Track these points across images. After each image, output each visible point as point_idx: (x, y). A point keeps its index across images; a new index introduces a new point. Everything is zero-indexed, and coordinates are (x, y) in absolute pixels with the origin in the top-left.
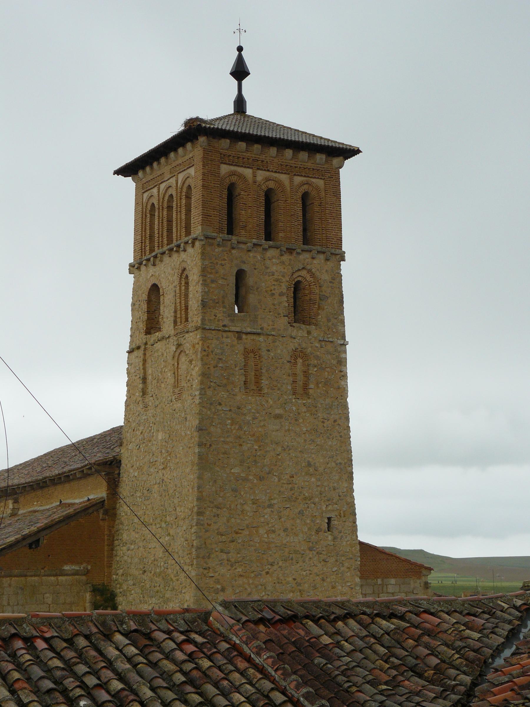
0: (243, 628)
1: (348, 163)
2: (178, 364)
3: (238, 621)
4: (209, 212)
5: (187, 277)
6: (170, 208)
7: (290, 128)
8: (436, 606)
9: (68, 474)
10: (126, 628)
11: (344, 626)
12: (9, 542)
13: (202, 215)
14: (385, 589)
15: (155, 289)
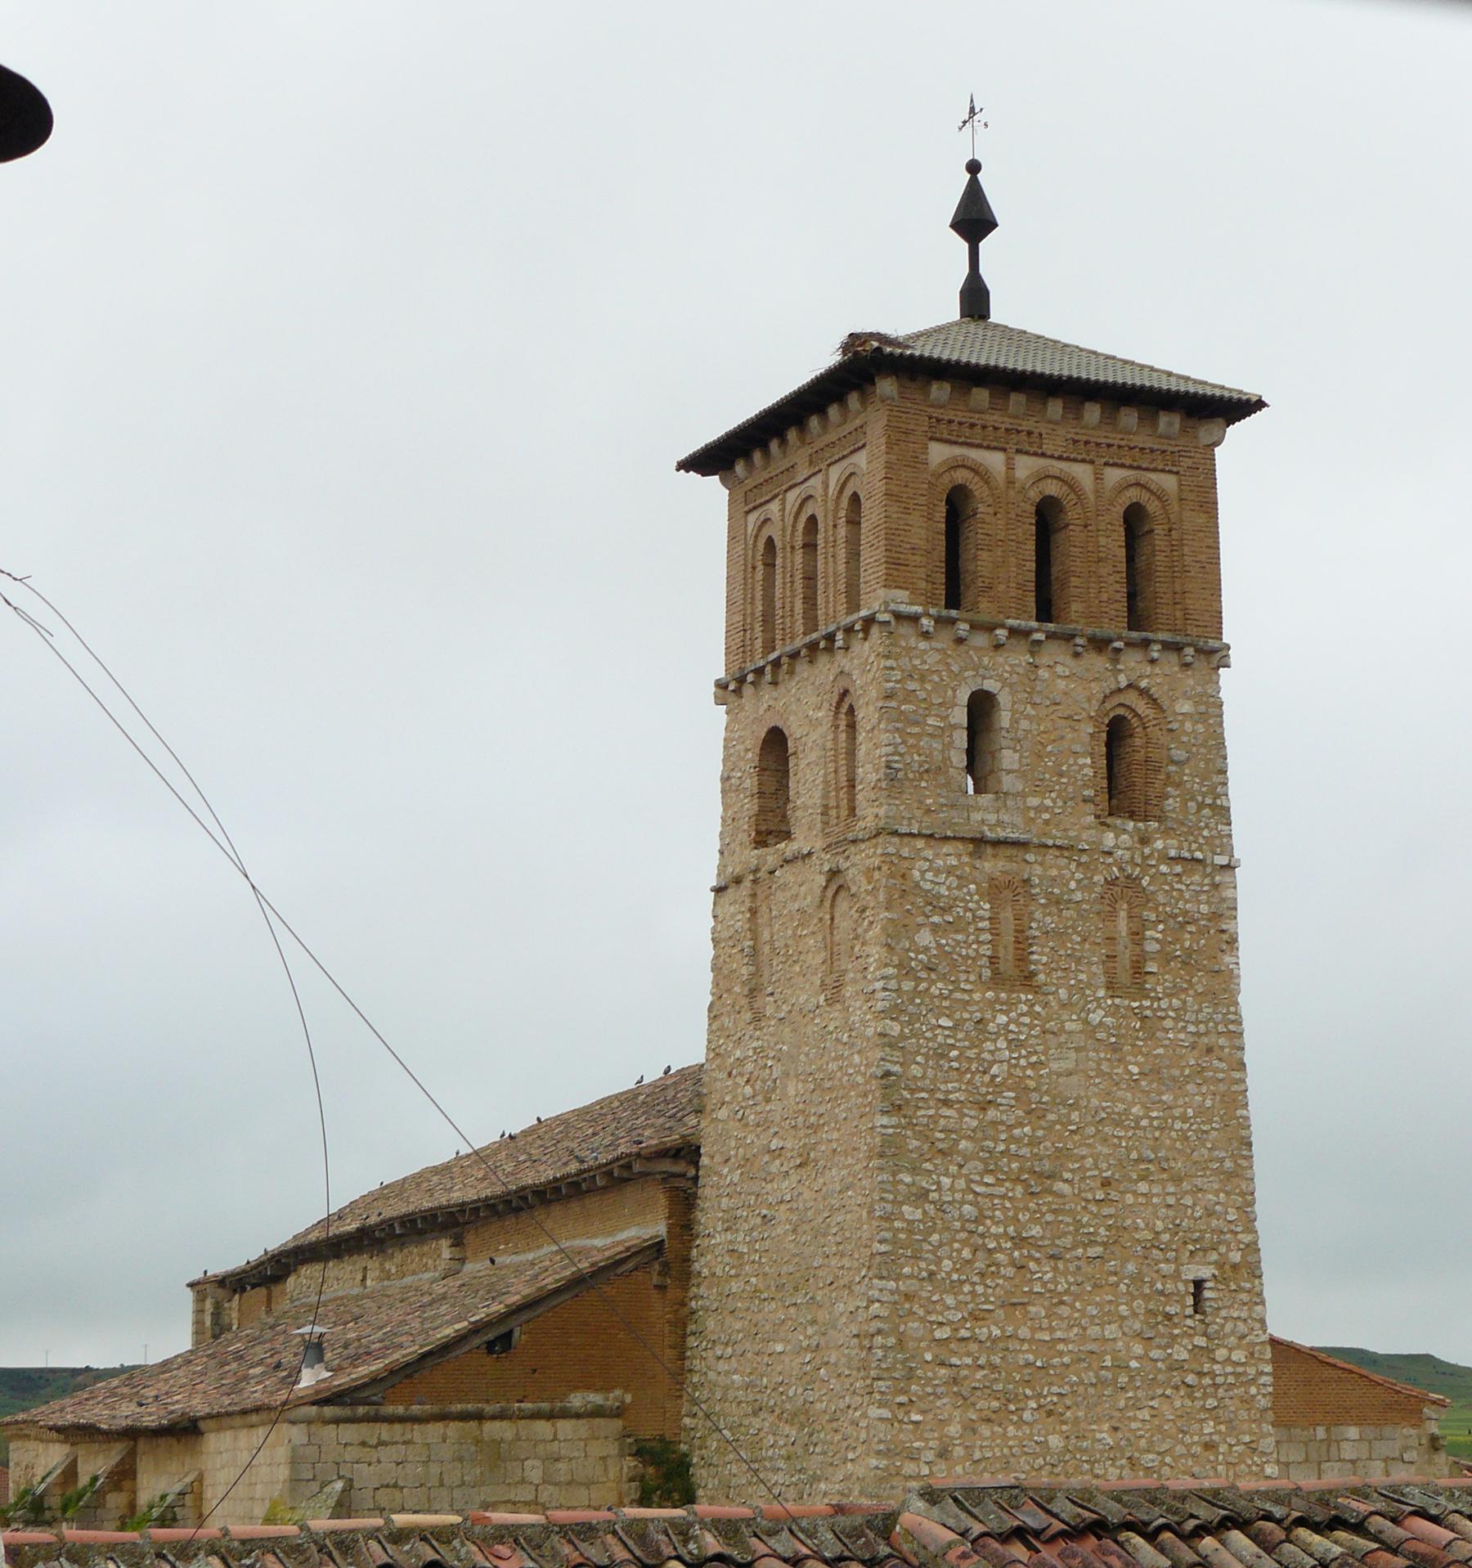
0: (975, 1552)
1: (1237, 433)
2: (832, 919)
3: (963, 1534)
4: (902, 556)
5: (851, 711)
6: (810, 547)
7: (1095, 353)
8: (1442, 1500)
9: (575, 1179)
10: (695, 1552)
11: (1219, 1546)
12: (439, 1339)
13: (886, 562)
14: (1334, 1449)
15: (775, 744)
